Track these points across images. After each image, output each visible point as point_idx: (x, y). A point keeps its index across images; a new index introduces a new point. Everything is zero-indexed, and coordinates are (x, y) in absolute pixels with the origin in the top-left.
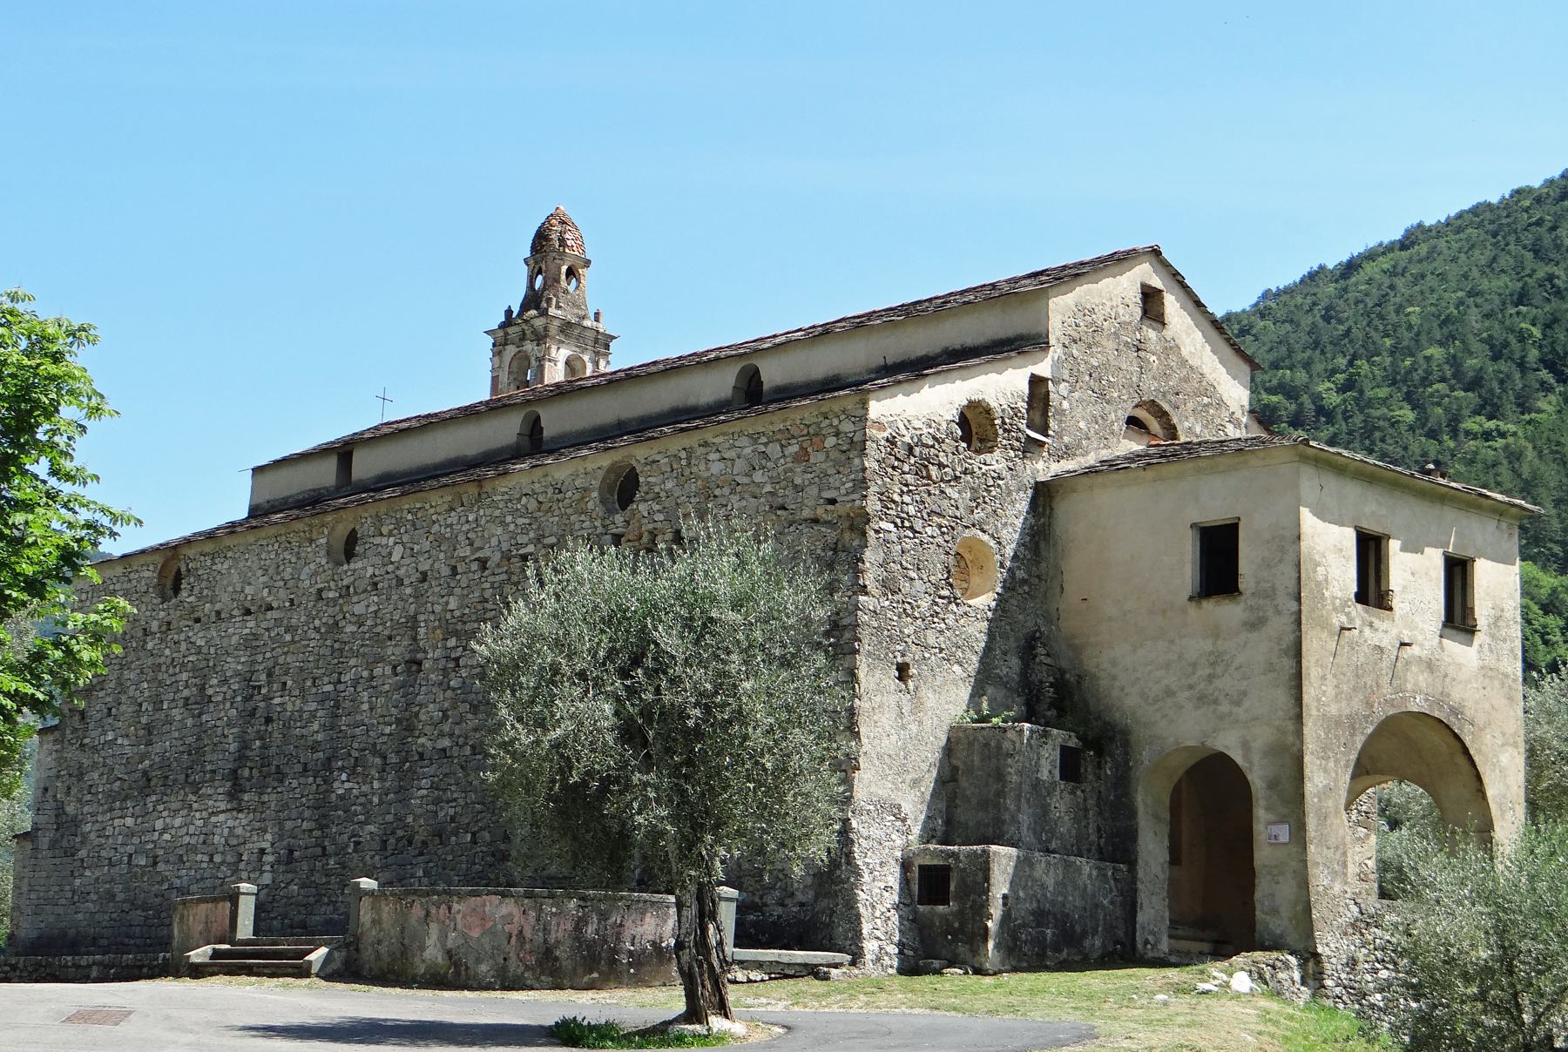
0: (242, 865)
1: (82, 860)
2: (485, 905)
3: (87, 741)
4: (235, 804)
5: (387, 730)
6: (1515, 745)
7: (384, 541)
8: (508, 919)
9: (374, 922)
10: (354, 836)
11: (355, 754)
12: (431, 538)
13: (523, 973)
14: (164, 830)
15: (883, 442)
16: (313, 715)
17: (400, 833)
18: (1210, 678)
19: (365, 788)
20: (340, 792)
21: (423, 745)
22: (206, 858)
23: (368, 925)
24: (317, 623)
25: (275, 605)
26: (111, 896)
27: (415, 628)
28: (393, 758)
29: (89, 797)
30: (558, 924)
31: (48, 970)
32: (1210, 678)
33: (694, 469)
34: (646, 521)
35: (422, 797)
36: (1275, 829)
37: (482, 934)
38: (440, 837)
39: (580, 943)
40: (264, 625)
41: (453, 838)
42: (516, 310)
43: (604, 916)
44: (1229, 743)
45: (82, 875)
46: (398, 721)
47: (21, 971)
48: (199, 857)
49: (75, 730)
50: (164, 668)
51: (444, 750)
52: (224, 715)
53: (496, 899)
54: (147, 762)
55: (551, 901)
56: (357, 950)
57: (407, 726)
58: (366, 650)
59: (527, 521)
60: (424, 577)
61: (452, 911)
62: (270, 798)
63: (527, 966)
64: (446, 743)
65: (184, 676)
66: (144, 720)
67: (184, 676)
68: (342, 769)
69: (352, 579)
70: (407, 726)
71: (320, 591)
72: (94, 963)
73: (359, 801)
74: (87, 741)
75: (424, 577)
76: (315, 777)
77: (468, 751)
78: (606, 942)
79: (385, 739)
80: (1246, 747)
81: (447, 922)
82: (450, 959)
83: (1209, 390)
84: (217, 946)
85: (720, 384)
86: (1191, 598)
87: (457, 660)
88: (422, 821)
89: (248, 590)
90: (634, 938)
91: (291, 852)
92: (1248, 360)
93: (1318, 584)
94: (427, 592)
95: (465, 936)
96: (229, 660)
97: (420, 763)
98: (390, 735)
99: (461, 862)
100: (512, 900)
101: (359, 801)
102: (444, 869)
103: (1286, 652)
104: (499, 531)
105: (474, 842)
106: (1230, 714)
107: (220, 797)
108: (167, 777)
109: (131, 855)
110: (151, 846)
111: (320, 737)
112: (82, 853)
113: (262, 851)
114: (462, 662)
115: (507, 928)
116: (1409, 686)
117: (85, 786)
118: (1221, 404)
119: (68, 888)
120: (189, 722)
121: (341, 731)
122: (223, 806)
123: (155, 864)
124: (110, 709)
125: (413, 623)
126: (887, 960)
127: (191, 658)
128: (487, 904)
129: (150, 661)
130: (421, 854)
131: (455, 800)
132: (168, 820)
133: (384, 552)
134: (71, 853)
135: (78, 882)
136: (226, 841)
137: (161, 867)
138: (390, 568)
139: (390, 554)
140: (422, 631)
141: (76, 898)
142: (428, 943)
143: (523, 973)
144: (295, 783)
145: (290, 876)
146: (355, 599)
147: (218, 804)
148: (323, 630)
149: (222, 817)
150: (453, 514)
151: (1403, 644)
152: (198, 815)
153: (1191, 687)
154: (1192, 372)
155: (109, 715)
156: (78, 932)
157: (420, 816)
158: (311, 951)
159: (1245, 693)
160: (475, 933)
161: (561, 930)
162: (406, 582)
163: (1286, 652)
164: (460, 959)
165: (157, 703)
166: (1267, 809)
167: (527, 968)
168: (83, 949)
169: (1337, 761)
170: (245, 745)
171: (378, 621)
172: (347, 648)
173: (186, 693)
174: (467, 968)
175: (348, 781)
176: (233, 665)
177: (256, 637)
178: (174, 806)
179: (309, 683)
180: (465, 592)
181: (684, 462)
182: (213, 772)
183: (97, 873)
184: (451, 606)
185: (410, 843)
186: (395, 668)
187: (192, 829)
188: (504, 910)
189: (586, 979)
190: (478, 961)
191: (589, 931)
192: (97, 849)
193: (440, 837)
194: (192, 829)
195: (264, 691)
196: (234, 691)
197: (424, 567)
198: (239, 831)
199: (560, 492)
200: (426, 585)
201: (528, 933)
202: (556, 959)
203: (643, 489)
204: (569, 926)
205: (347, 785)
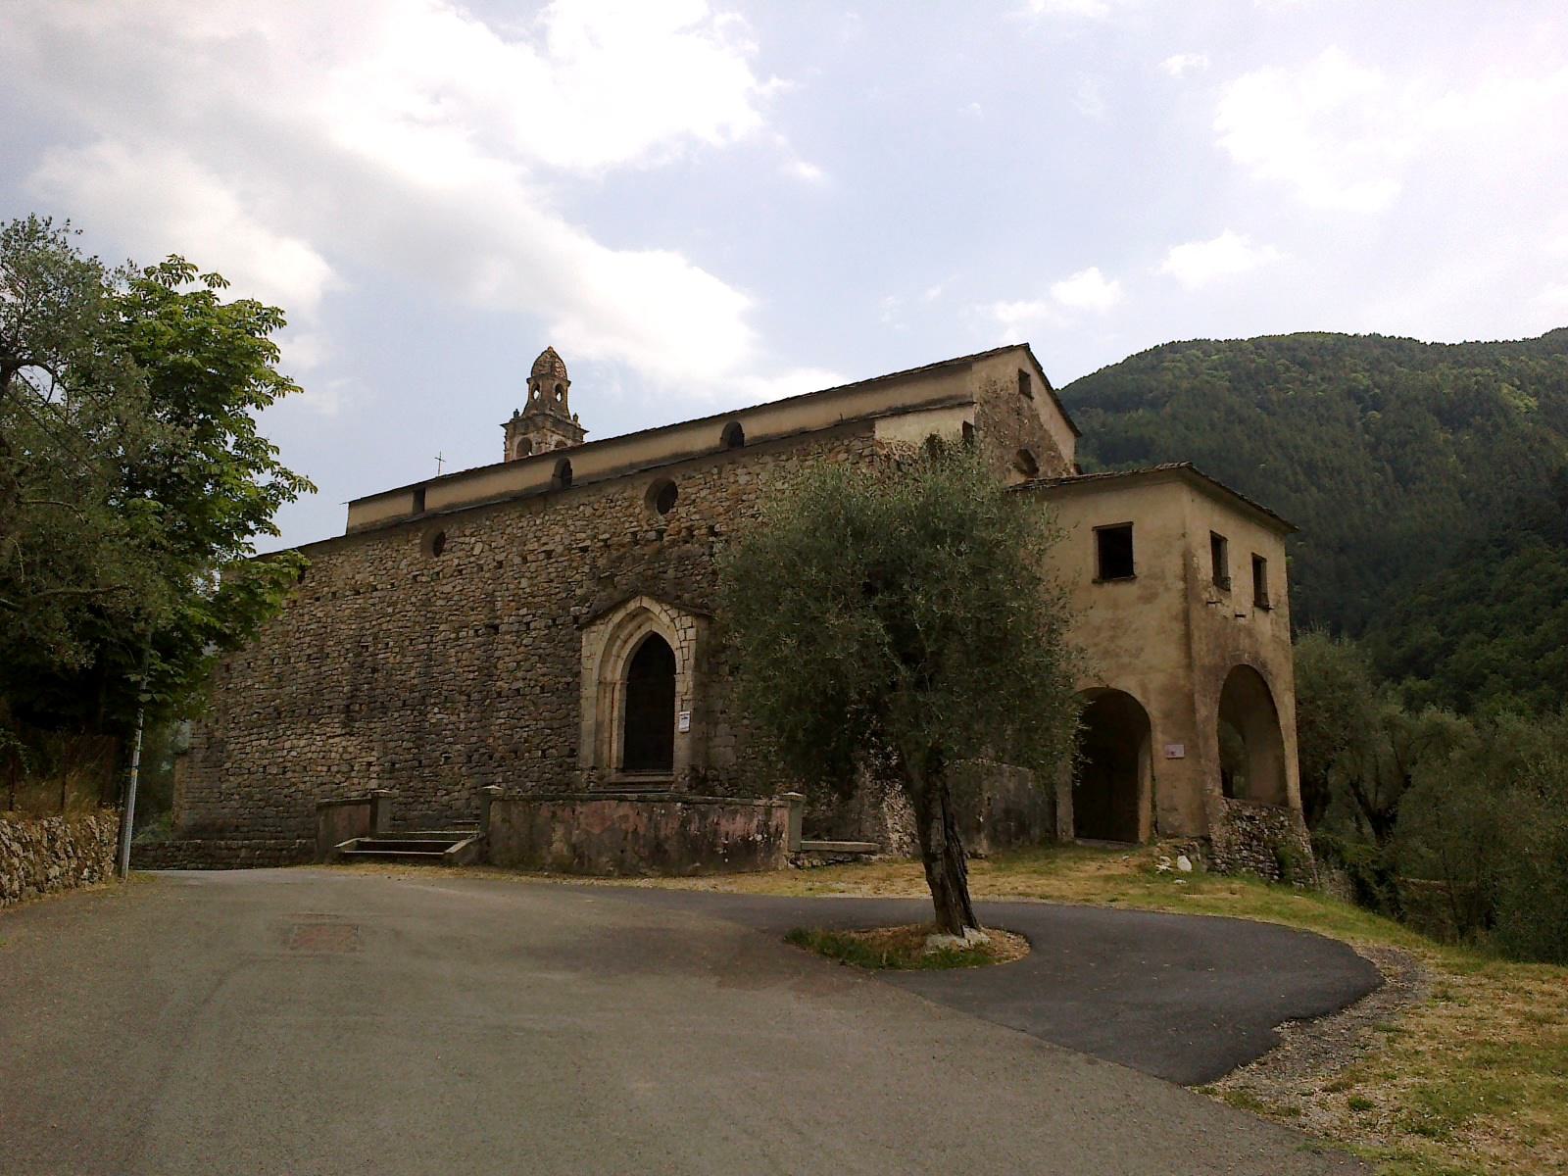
0: (353, 774)
1: (227, 770)
2: (604, 808)
3: (231, 686)
4: (348, 730)
5: (471, 676)
6: (1290, 690)
7: (467, 540)
8: (625, 818)
9: (504, 820)
10: (446, 753)
11: (445, 693)
12: (505, 537)
13: (638, 863)
14: (292, 749)
15: (883, 458)
16: (410, 666)
17: (482, 750)
18: (1112, 639)
19: (454, 718)
20: (433, 721)
21: (500, 687)
22: (325, 769)
23: (499, 823)
24: (413, 599)
25: (379, 587)
26: (249, 796)
27: (493, 603)
28: (475, 696)
29: (232, 726)
30: (667, 824)
31: (206, 851)
32: (1112, 639)
33: (724, 481)
34: (685, 520)
35: (501, 724)
36: (1172, 748)
37: (603, 832)
38: (516, 753)
39: (685, 838)
40: (371, 601)
41: (527, 754)
42: (521, 412)
43: (704, 816)
44: (1128, 684)
45: (228, 780)
46: (480, 670)
47: (185, 851)
48: (319, 768)
49: (223, 678)
50: (291, 634)
51: (518, 690)
52: (339, 667)
53: (614, 803)
54: (278, 701)
55: (660, 804)
56: (488, 844)
57: (488, 672)
58: (454, 618)
59: (585, 523)
60: (500, 564)
61: (576, 813)
62: (377, 726)
63: (641, 857)
64: (520, 684)
65: (308, 639)
66: (276, 671)
67: (308, 639)
68: (435, 704)
69: (441, 567)
70: (488, 672)
71: (415, 577)
72: (243, 847)
73: (448, 727)
74: (231, 686)
75: (500, 564)
76: (412, 710)
77: (538, 690)
78: (705, 836)
79: (469, 682)
80: (1144, 689)
81: (572, 821)
82: (575, 851)
83: (1053, 447)
84: (362, 840)
85: (712, 438)
86: (1094, 582)
87: (528, 624)
88: (500, 742)
89: (357, 577)
90: (727, 834)
91: (393, 764)
92: (1077, 434)
93: (1195, 569)
94: (502, 575)
95: (588, 833)
96: (343, 627)
97: (498, 700)
98: (473, 679)
99: (534, 772)
100: (628, 803)
101: (448, 727)
102: (520, 777)
103: (1175, 618)
104: (562, 531)
105: (544, 756)
106: (1130, 663)
107: (336, 725)
108: (294, 711)
109: (265, 767)
110: (281, 760)
111: (416, 681)
112: (228, 765)
113: (370, 764)
114: (532, 625)
115: (623, 827)
116: (1241, 648)
117: (230, 718)
118: (1060, 457)
119: (216, 790)
120: (312, 672)
121: (433, 677)
122: (339, 731)
123: (284, 773)
124: (249, 663)
125: (490, 599)
126: (905, 848)
127: (312, 627)
128: (607, 807)
129: (280, 629)
130: (500, 766)
131: (528, 726)
132: (295, 741)
133: (467, 548)
134: (219, 764)
135: (224, 786)
136: (341, 756)
137: (289, 775)
138: (472, 559)
139: (472, 549)
140: (499, 605)
141: (222, 798)
142: (554, 839)
143: (638, 863)
144: (396, 715)
145: (392, 782)
146: (444, 582)
147: (334, 730)
148: (418, 604)
149: (337, 740)
150: (523, 520)
151: (1237, 616)
152: (318, 738)
153: (1096, 645)
154: (1046, 435)
155: (249, 667)
156: (224, 822)
157: (499, 738)
158: (452, 845)
159: (1142, 649)
160: (596, 831)
161: (669, 828)
162: (485, 568)
163: (1175, 618)
164: (583, 853)
165: (287, 660)
166: (1163, 732)
167: (642, 859)
168: (228, 835)
169: (1211, 698)
170: (356, 689)
171: (463, 597)
172: (438, 617)
173: (309, 651)
174: (590, 860)
175: (440, 713)
176: (347, 630)
177: (364, 610)
178: (299, 731)
179: (407, 643)
180: (534, 575)
181: (715, 477)
182: (331, 707)
183: (240, 780)
184: (522, 586)
185: (491, 758)
186: (476, 631)
187: (313, 748)
188: (621, 812)
189: (690, 868)
190: (599, 854)
191: (692, 829)
192: (239, 762)
193: (516, 753)
194: (313, 748)
195: (370, 649)
196: (347, 650)
197: (500, 557)
198: (350, 749)
199: (612, 502)
200: (502, 571)
201: (642, 830)
202: (666, 851)
203: (681, 496)
204: (676, 825)
205: (439, 716)
